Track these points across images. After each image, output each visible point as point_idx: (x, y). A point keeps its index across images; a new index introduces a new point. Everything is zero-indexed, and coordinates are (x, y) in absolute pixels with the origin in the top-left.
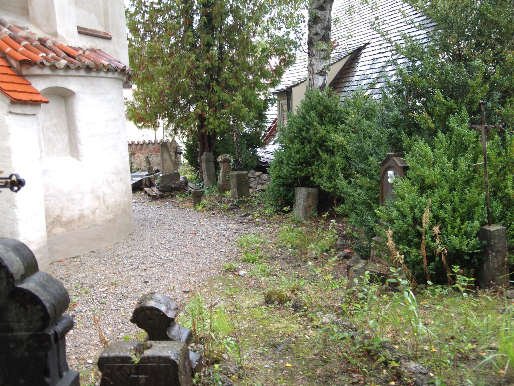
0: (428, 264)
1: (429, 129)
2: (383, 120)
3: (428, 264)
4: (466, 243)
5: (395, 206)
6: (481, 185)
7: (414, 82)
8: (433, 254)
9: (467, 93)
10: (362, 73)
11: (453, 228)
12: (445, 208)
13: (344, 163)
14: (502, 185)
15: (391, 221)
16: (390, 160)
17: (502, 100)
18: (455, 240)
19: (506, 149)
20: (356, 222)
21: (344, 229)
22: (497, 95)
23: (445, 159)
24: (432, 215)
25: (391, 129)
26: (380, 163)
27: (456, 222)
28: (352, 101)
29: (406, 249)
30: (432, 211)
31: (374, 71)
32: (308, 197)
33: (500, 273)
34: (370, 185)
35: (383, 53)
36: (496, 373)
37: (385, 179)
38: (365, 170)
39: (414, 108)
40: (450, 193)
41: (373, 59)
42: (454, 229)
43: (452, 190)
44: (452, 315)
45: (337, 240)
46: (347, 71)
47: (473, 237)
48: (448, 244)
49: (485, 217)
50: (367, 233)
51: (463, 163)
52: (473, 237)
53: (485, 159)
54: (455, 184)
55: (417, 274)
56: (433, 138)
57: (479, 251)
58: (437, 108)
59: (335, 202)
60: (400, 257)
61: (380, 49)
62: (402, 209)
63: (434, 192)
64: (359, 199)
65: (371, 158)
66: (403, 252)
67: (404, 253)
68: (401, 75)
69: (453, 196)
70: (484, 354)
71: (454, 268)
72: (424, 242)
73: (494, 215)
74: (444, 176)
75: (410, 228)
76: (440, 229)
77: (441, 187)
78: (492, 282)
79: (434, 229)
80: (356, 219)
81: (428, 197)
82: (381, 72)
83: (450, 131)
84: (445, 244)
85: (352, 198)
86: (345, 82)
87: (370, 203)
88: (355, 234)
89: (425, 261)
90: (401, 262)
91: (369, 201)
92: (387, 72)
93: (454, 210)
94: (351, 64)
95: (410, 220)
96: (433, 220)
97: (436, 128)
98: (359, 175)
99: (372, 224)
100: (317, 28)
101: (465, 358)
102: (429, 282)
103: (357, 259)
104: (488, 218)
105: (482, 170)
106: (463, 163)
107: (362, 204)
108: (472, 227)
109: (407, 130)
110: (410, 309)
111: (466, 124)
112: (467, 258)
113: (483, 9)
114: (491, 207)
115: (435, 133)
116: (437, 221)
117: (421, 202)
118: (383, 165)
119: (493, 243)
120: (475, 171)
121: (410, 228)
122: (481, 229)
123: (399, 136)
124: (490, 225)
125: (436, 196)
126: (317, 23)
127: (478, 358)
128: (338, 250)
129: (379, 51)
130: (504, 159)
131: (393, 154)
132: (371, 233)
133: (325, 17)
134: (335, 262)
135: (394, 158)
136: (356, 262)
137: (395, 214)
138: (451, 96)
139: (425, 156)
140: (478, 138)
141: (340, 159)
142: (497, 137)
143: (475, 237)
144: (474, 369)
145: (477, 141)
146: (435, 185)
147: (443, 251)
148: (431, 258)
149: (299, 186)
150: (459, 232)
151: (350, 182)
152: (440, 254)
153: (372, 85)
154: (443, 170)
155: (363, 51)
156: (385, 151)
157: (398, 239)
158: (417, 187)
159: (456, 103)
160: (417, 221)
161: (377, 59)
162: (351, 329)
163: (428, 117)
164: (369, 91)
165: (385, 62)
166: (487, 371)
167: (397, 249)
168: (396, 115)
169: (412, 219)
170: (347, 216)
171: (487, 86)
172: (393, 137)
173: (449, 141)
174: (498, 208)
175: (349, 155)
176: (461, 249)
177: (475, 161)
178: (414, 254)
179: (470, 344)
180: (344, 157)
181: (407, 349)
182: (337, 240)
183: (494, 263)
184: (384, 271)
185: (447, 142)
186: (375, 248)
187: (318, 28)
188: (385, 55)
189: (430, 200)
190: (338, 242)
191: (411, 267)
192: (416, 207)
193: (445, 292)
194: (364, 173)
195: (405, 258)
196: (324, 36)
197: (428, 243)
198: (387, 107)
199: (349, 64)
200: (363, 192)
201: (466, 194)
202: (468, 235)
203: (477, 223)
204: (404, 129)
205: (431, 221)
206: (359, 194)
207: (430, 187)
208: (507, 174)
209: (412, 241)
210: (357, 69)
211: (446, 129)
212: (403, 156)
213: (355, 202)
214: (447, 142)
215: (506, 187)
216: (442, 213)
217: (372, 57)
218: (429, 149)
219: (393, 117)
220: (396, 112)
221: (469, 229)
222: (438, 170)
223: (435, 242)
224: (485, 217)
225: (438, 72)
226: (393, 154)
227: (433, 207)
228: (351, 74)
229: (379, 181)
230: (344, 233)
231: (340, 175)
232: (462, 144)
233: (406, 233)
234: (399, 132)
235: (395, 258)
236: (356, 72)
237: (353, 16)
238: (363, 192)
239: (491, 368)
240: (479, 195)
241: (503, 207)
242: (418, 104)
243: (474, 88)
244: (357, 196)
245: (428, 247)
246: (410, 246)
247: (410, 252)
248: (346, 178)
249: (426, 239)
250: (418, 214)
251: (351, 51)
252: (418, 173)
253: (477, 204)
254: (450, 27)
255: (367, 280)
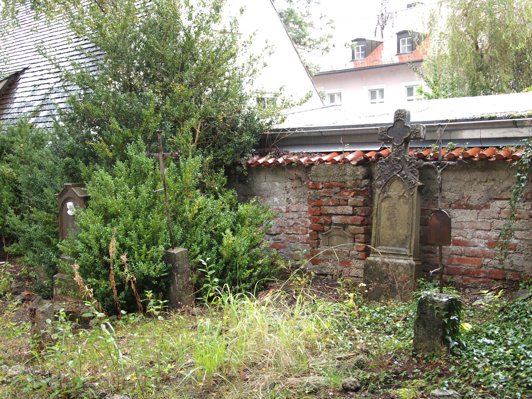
0: (118, 294)
1: (107, 157)
2: (57, 149)
3: (118, 294)
4: (153, 267)
5: (79, 239)
6: (162, 210)
7: (88, 110)
8: (122, 283)
9: (141, 123)
10: (22, 99)
11: (140, 255)
12: (130, 236)
13: (12, 198)
14: (181, 209)
15: (76, 255)
16: (69, 191)
17: (173, 129)
18: (143, 267)
19: (182, 176)
20: (34, 261)
21: (17, 270)
22: (169, 125)
23: (126, 186)
24: (118, 243)
25: (67, 159)
26: (57, 194)
27: (142, 249)
28: (16, 129)
29: (94, 281)
30: (118, 240)
31: (37, 98)
33: (186, 293)
34: (47, 219)
35: (45, 79)
36: (196, 386)
37: (64, 211)
38: (40, 203)
39: (89, 137)
40: (134, 221)
41: (35, 86)
42: (141, 256)
43: (135, 217)
44: (148, 340)
45: (11, 282)
46: (5, 97)
47: (159, 262)
48: (136, 271)
49: (168, 241)
50: (47, 271)
51: (144, 190)
52: (159, 262)
53: (164, 185)
54: (138, 211)
55: (107, 305)
56: (112, 167)
57: (166, 274)
58: (114, 137)
59: (4, 241)
60: (88, 291)
61: (42, 75)
62: (87, 241)
63: (118, 221)
64: (36, 235)
65: (46, 190)
66: (92, 285)
67: (92, 286)
68: (73, 102)
69: (137, 223)
70: (182, 372)
71: (147, 293)
72: (112, 272)
73: (176, 238)
74: (127, 204)
75: (97, 260)
76: (128, 257)
77: (125, 215)
78: (179, 303)
79: (122, 257)
80: (34, 257)
81: (112, 226)
82: (45, 99)
83: (128, 159)
84: (132, 271)
85: (27, 235)
86: (3, 109)
87: (49, 238)
88: (32, 274)
89: (115, 292)
90: (90, 296)
91: (48, 236)
92: (51, 99)
93: (140, 237)
94: (9, 89)
95: (96, 251)
96: (120, 249)
97: (114, 157)
98: (34, 209)
99: (54, 259)
101: (166, 380)
102: (123, 312)
103: (40, 300)
104: (171, 242)
105: (162, 197)
106: (144, 190)
107: (40, 240)
108: (157, 252)
109: (84, 159)
110: (109, 341)
111: (143, 152)
112: (155, 282)
113: (150, 42)
114: (173, 231)
115: (114, 161)
116: (124, 250)
117: (106, 231)
118: (61, 196)
119: (177, 265)
120: (155, 198)
121: (97, 260)
122: (167, 253)
123: (77, 166)
124: (173, 249)
125: (121, 225)
127: (177, 376)
128: (16, 293)
129: (41, 77)
130: (180, 185)
131: (71, 184)
132: (53, 269)
134: (17, 306)
135: (73, 188)
136: (40, 303)
137: (80, 246)
138: (126, 125)
139: (106, 185)
140: (155, 166)
141: (7, 193)
142: (172, 164)
143: (161, 261)
144: (176, 388)
145: (155, 168)
146: (118, 214)
147: (132, 278)
148: (120, 288)
150: (146, 258)
151: (22, 218)
152: (129, 282)
153: (36, 113)
154: (125, 198)
155: (22, 76)
156: (61, 182)
157: (85, 272)
158: (101, 217)
159: (132, 132)
160: (104, 252)
161: (39, 85)
162: (45, 376)
163: (105, 145)
164: (33, 120)
165: (48, 89)
166: (188, 386)
167: (85, 284)
168: (71, 144)
169: (99, 250)
170: (20, 255)
171: (160, 116)
172: (70, 166)
173: (129, 170)
174: (179, 232)
175: (20, 188)
176: (149, 274)
177: (154, 187)
178: (103, 286)
179: (169, 365)
180: (11, 191)
181: (108, 384)
182: (11, 282)
183: (179, 284)
184: (72, 308)
185: (126, 170)
186: (60, 286)
188: (47, 81)
189: (115, 229)
190: (13, 285)
191: (100, 300)
192: (102, 237)
193: (137, 319)
194: (41, 206)
195: (94, 291)
197: (116, 273)
198: (60, 135)
199: (7, 90)
200: (40, 227)
201: (149, 220)
202: (154, 260)
203: (161, 248)
204: (81, 158)
205: (118, 250)
206: (35, 230)
207: (114, 216)
208: (184, 199)
209: (100, 272)
210: (16, 95)
211: (125, 158)
212: (84, 186)
213: (31, 239)
214: (126, 170)
215: (184, 211)
216: (128, 241)
217: (33, 83)
218: (109, 178)
219: (69, 147)
220: (71, 140)
221: (155, 254)
222: (120, 198)
223: (123, 270)
224: (168, 241)
225: (112, 101)
226: (71, 184)
227: (119, 236)
228: (9, 101)
229: (58, 215)
230: (18, 274)
231: (10, 211)
232: (142, 172)
233: (94, 265)
234: (76, 161)
235: (84, 292)
236: (15, 98)
237: (6, 37)
238: (40, 226)
239: (191, 384)
240: (161, 220)
241: (183, 230)
242: (92, 133)
243: (148, 117)
244: (33, 232)
245: (117, 277)
246: (98, 278)
247: (98, 284)
248: (17, 212)
249: (114, 269)
250: (104, 245)
251: (8, 75)
252: (101, 203)
253: (160, 229)
254: (119, 57)
255: (63, 318)
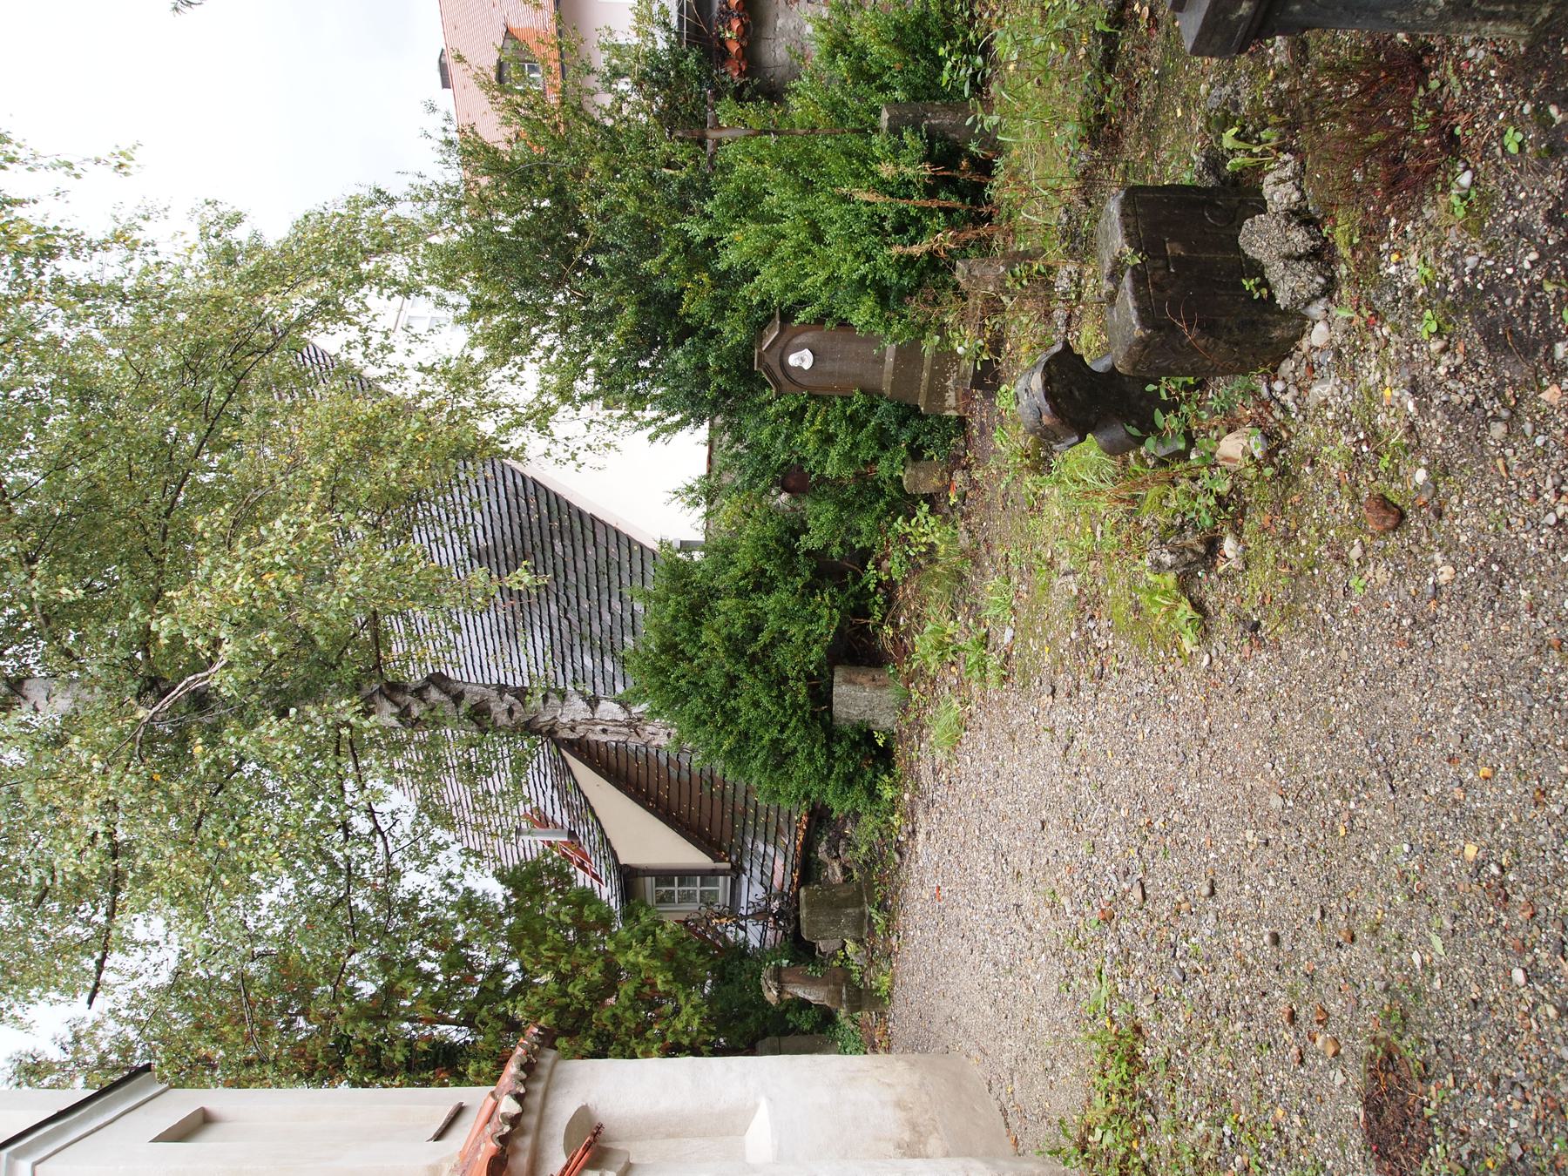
32: (854, 683)
46: (594, 751)
100: (498, 709)
126: (489, 708)
133: (477, 694)
149: (830, 710)
187: (499, 709)
196: (516, 697)
